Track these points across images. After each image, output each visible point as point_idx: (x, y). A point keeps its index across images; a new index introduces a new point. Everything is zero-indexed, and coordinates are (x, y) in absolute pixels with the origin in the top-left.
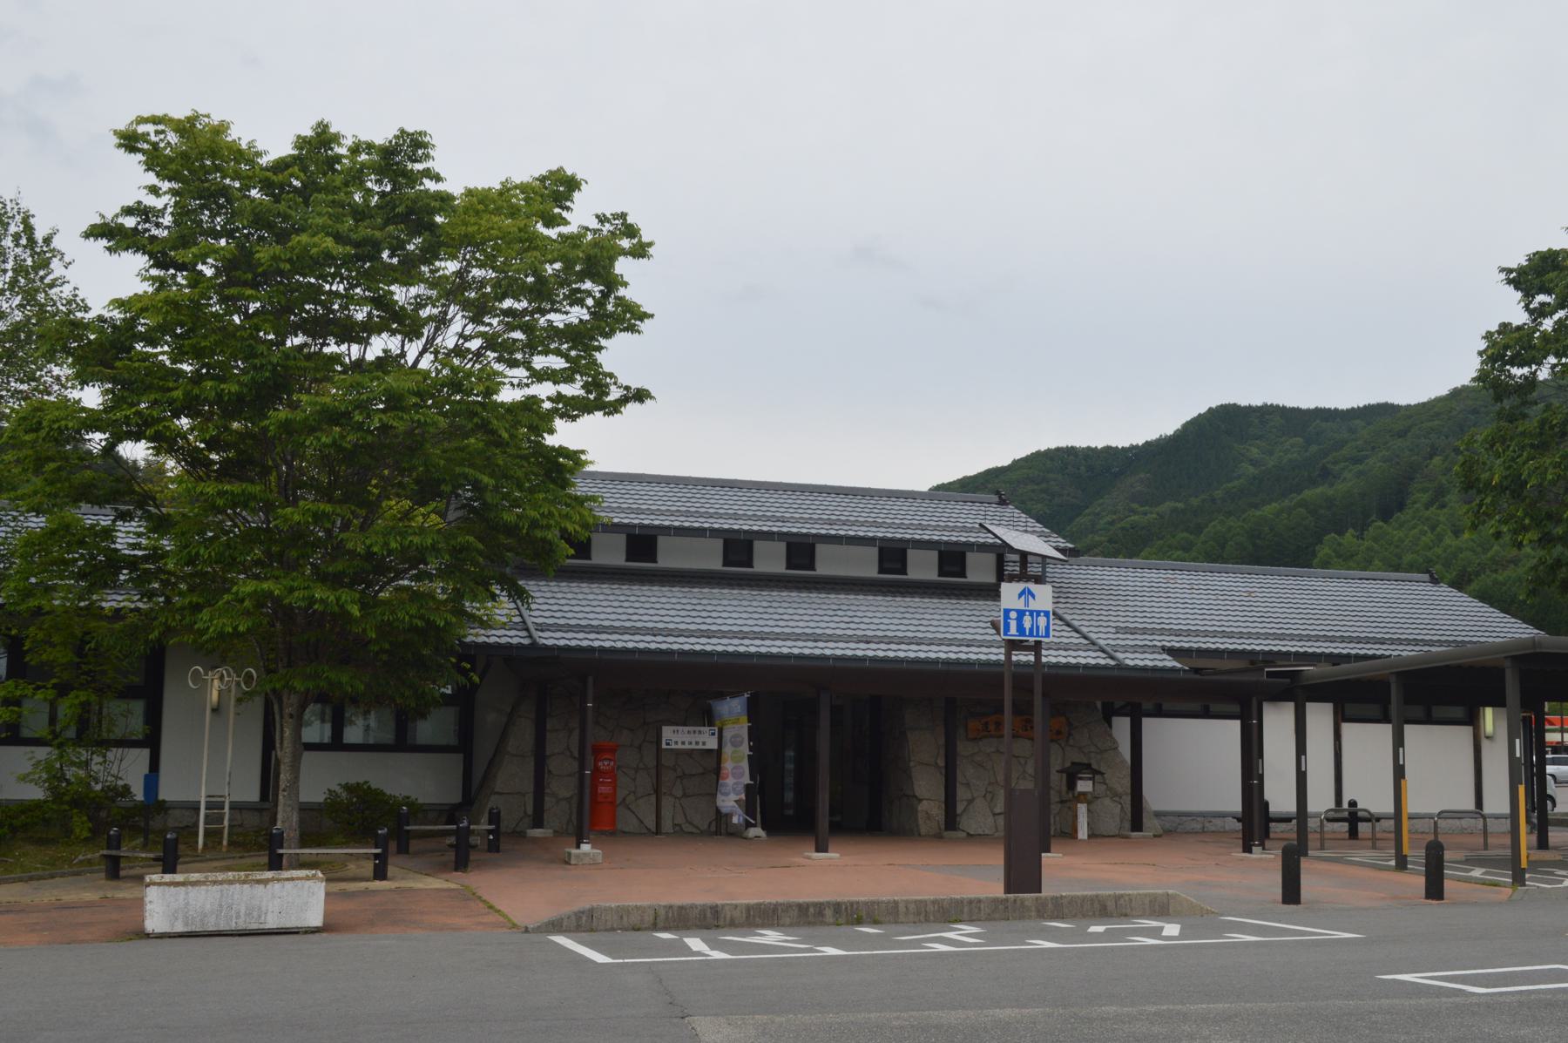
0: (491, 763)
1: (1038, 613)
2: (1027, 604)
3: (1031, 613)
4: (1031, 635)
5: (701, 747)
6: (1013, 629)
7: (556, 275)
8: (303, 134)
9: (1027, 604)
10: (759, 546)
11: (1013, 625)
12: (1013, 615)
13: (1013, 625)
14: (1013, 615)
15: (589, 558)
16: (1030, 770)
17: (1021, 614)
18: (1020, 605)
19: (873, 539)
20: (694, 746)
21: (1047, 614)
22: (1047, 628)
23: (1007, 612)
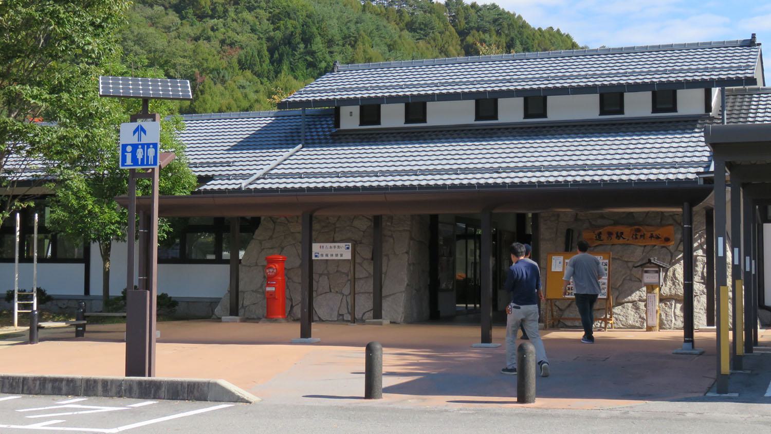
0: (597, 246)
1: (148, 145)
2: (139, 139)
3: (143, 145)
4: (142, 164)
5: (339, 258)
6: (129, 160)
7: (100, 19)
8: (477, 3)
9: (139, 139)
10: (384, 108)
11: (129, 157)
12: (129, 149)
13: (129, 157)
14: (129, 149)
15: (676, 111)
16: (402, 305)
17: (135, 147)
18: (134, 140)
19: (356, 99)
20: (329, 258)
21: (155, 146)
22: (155, 157)
23: (124, 146)
